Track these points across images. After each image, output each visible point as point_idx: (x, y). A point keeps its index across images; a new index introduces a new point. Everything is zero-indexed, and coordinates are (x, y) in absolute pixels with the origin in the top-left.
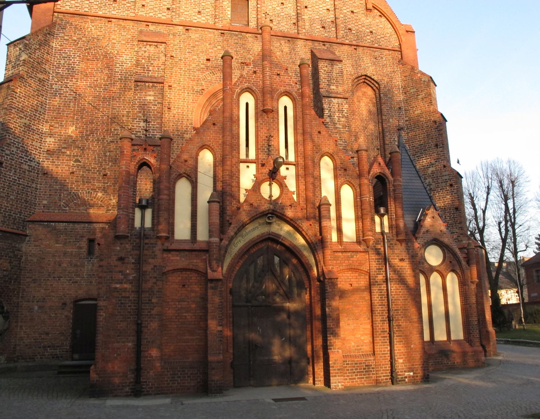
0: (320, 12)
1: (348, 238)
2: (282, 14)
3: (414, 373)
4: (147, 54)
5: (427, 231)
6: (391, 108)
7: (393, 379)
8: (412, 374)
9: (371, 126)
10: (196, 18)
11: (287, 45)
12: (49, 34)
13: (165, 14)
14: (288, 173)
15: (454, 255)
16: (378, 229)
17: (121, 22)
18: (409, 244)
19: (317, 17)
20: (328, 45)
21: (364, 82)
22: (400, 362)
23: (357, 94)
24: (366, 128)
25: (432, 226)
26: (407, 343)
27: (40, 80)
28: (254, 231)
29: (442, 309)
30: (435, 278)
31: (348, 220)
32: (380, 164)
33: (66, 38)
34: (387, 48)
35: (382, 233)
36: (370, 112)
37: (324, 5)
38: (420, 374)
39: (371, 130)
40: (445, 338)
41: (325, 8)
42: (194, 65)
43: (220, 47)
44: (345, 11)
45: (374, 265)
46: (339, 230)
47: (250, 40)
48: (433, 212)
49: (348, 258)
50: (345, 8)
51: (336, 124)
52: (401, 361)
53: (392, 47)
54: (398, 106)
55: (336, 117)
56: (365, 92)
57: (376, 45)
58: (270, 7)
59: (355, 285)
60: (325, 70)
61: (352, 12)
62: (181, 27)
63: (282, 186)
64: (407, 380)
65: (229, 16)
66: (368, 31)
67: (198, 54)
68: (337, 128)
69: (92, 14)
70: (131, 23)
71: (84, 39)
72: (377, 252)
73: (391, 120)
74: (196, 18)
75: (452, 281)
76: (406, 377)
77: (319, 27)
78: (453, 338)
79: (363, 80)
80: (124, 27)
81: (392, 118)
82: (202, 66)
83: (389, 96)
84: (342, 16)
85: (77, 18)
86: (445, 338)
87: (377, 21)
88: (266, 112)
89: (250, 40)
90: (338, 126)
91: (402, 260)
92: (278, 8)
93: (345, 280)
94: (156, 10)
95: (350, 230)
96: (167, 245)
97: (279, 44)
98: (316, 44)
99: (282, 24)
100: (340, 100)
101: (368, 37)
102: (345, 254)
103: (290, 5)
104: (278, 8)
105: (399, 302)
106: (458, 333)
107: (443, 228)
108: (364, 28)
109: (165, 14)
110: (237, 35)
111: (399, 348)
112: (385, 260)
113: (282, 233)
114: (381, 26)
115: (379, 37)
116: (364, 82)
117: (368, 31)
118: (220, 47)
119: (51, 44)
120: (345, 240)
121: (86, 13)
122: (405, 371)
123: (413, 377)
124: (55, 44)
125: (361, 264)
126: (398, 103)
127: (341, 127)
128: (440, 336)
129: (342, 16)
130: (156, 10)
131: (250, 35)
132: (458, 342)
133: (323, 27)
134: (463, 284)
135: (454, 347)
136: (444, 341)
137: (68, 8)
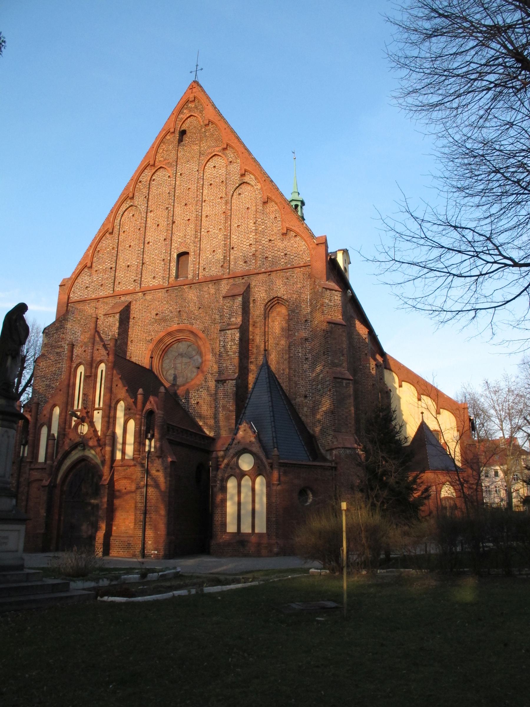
0: (244, 249)
1: (129, 456)
2: (213, 260)
3: (307, 571)
4: (108, 324)
5: (239, 442)
6: (298, 322)
7: (144, 556)
8: (156, 552)
9: (283, 342)
10: (152, 282)
11: (213, 287)
12: (64, 320)
13: (132, 285)
14: (98, 416)
15: (261, 461)
16: (147, 449)
17: (105, 300)
18: (164, 459)
19: (241, 254)
20: (246, 278)
21: (278, 303)
22: (149, 543)
23: (272, 315)
24: (278, 344)
25: (243, 438)
26: (156, 529)
27: (57, 353)
28: (75, 455)
29: (250, 507)
30: (246, 481)
31: (130, 444)
32: (151, 402)
33: (74, 319)
34: (299, 265)
35: (149, 452)
36: (282, 329)
37: (248, 241)
38: (162, 553)
39: (283, 345)
40: (250, 531)
41: (248, 244)
42: (147, 321)
43: (165, 302)
44: (263, 242)
45: (139, 475)
46: (123, 453)
47: (186, 290)
48: (245, 426)
49: (124, 470)
50: (264, 239)
51: (229, 351)
52: (150, 542)
53: (304, 263)
54: (304, 319)
55: (229, 346)
56: (279, 312)
57: (289, 266)
58: (204, 257)
59: (128, 488)
60: (227, 306)
61: (270, 240)
62: (141, 293)
63: (92, 424)
64: (152, 556)
65: (174, 274)
66: (282, 254)
67: (150, 312)
68: (228, 355)
69: (89, 298)
70: (110, 299)
71: (84, 318)
72: (142, 465)
73: (296, 334)
74: (152, 282)
75: (261, 484)
76: (152, 554)
77: (241, 263)
78: (257, 531)
79: (277, 301)
80: (107, 303)
81: (298, 332)
82: (153, 320)
83: (297, 311)
84: (260, 247)
85: (81, 304)
86: (250, 531)
87: (292, 242)
88: (91, 377)
89: (186, 290)
90: (230, 353)
91: (158, 471)
92: (210, 256)
93: (121, 485)
94: (127, 283)
95: (130, 450)
96: (33, 466)
97: (207, 288)
98: (237, 280)
99: (213, 269)
100: (233, 330)
101: (282, 260)
102: (122, 468)
103: (219, 251)
104: (210, 256)
105: (153, 501)
106: (261, 527)
107: (253, 439)
108: (279, 253)
109: (132, 285)
110: (177, 289)
111: (149, 533)
112: (148, 472)
113: (91, 455)
114: (296, 246)
115: (293, 257)
116: (278, 303)
117: (282, 254)
118: (165, 302)
119: (66, 326)
120: (126, 458)
121: (86, 299)
122: (152, 550)
123: (157, 554)
124: (69, 326)
125: (132, 474)
126: (305, 316)
127: (232, 353)
128: (246, 529)
129: (260, 247)
130: (127, 283)
131: (187, 286)
132: (260, 535)
133: (245, 262)
134: (269, 485)
135: (253, 539)
136: (249, 533)
137: (76, 298)
